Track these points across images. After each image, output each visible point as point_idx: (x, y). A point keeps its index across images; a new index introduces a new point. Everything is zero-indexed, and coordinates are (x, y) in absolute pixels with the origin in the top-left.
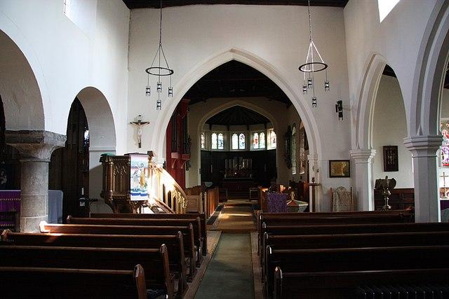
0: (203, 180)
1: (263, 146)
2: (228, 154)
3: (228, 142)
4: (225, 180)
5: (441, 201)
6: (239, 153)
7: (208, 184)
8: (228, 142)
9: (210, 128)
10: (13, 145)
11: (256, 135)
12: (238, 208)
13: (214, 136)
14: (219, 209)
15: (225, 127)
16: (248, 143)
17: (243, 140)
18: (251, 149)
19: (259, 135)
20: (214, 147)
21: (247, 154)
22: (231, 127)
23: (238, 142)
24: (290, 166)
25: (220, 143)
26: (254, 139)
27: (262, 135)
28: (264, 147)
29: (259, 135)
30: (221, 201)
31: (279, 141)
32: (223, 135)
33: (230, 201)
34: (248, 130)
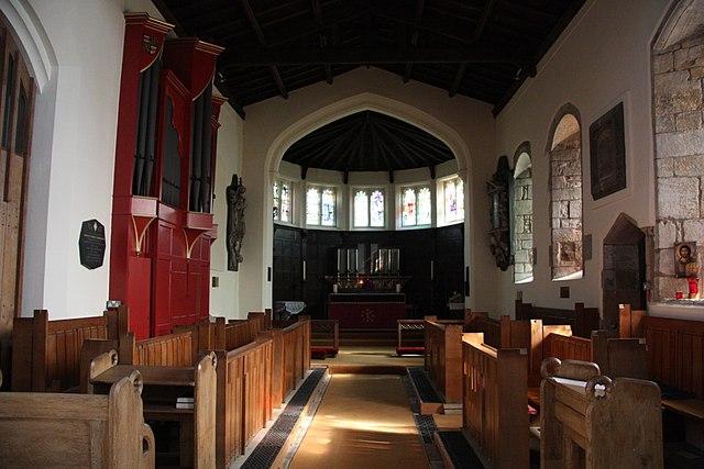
0: (278, 296)
1: (424, 221)
2: (347, 238)
3: (344, 211)
4: (335, 298)
5: (403, 330)
6: (369, 238)
7: (294, 307)
8: (344, 211)
9: (304, 177)
10: (558, 380)
11: (410, 194)
12: (369, 391)
13: (312, 195)
14: (304, 392)
15: (338, 175)
16: (391, 212)
17: (381, 207)
18: (398, 227)
19: (417, 192)
20: (312, 220)
21: (388, 237)
22: (353, 175)
23: (367, 212)
24: (505, 261)
25: (325, 212)
26: (406, 204)
27: (425, 194)
28: (429, 221)
29: (417, 192)
30: (317, 355)
31: (475, 202)
32: (335, 193)
33: (349, 356)
34: (392, 181)
